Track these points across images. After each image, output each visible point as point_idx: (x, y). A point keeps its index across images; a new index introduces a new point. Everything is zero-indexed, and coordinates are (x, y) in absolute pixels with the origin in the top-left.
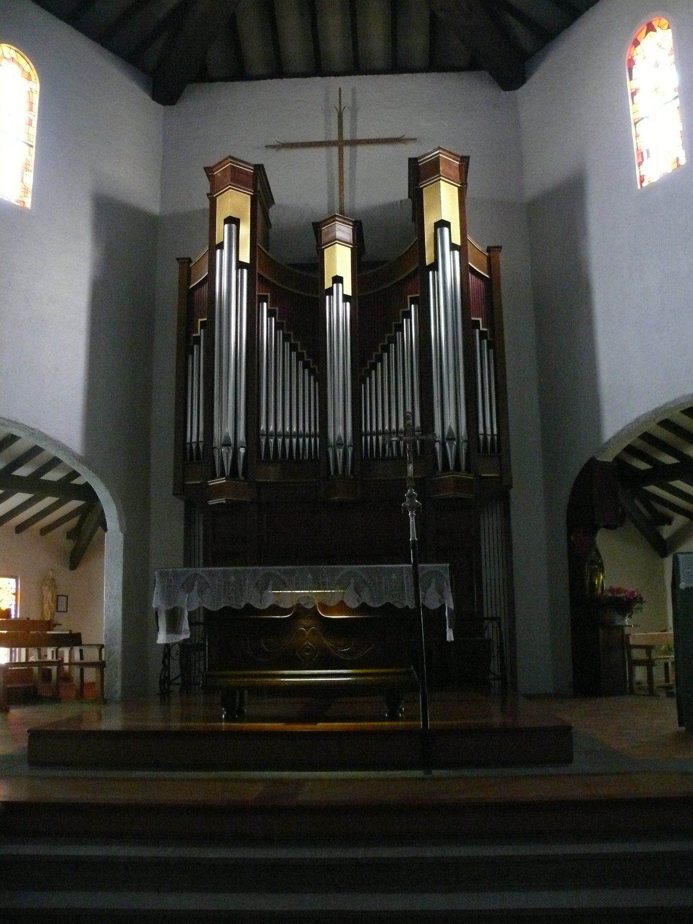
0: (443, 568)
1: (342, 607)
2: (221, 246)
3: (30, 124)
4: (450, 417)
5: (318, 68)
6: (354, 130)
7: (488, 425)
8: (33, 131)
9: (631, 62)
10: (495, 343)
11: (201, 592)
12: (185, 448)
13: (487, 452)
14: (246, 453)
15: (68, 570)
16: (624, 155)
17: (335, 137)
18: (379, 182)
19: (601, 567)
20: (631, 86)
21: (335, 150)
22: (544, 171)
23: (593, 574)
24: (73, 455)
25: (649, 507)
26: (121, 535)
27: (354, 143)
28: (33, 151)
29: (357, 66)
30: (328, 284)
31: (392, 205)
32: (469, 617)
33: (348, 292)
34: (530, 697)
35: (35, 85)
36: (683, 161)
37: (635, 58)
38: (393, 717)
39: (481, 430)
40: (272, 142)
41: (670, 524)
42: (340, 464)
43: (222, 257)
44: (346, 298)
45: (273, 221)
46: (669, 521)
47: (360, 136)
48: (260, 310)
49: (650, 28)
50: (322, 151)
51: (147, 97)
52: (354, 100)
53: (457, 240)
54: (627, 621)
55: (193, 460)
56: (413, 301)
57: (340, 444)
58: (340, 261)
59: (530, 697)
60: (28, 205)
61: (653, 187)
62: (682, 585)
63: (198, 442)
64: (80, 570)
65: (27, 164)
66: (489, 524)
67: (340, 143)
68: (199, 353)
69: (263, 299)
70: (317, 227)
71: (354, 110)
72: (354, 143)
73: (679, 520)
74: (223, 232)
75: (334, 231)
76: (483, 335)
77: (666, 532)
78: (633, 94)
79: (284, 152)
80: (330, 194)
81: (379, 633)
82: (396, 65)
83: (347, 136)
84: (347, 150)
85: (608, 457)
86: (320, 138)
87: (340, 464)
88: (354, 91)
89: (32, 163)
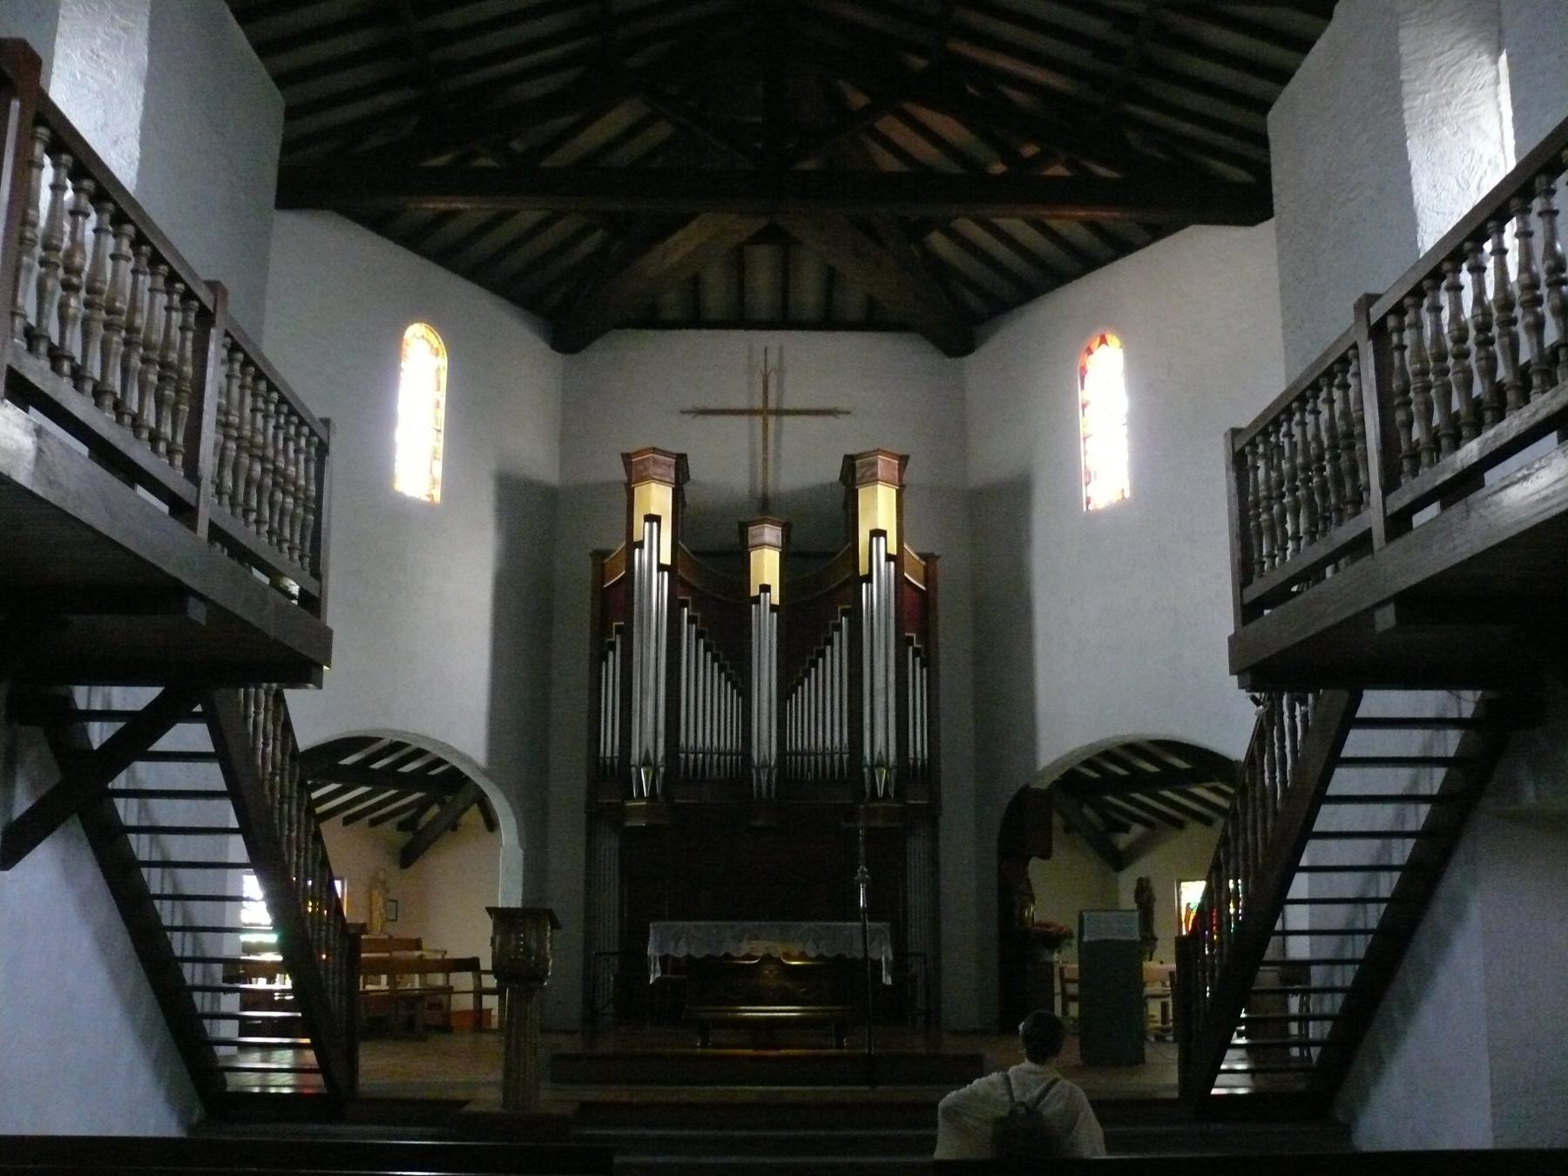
0: (884, 925)
1: (802, 956)
2: (640, 545)
3: (438, 406)
4: (880, 739)
5: (740, 320)
6: (780, 397)
7: (918, 744)
8: (441, 414)
9: (1083, 371)
10: (927, 630)
11: (688, 944)
12: (597, 764)
13: (919, 777)
14: (665, 774)
15: (396, 867)
16: (1070, 474)
17: (759, 404)
18: (805, 463)
19: (1032, 899)
20: (1083, 396)
21: (759, 420)
22: (991, 461)
23: (1024, 906)
24: (478, 768)
25: (1103, 816)
26: (520, 851)
27: (780, 412)
28: (441, 436)
29: (784, 320)
30: (754, 591)
31: (823, 487)
32: (900, 965)
33: (776, 600)
34: (955, 1033)
35: (443, 362)
36: (1127, 494)
37: (1088, 367)
38: (840, 1046)
39: (911, 755)
40: (688, 406)
41: (1127, 831)
42: (764, 786)
43: (641, 557)
44: (773, 608)
45: (688, 500)
46: (1126, 829)
47: (787, 405)
48: (681, 614)
49: (1103, 341)
50: (743, 421)
51: (543, 346)
52: (781, 359)
53: (893, 550)
54: (1056, 957)
55: (609, 777)
56: (844, 613)
57: (766, 765)
58: (767, 566)
59: (955, 1033)
60: (437, 498)
61: (1098, 514)
62: (1086, 939)
63: (612, 758)
64: (412, 870)
65: (435, 452)
66: (916, 846)
67: (765, 412)
68: (614, 660)
69: (684, 604)
70: (743, 529)
71: (781, 371)
72: (780, 412)
73: (1137, 830)
74: (641, 529)
75: (762, 534)
76: (916, 653)
77: (1123, 841)
78: (1084, 406)
79: (700, 421)
80: (753, 473)
81: (836, 979)
82: (828, 321)
83: (772, 405)
84: (772, 420)
85: (1043, 784)
86: (742, 405)
87: (764, 786)
88: (781, 348)
89: (441, 451)
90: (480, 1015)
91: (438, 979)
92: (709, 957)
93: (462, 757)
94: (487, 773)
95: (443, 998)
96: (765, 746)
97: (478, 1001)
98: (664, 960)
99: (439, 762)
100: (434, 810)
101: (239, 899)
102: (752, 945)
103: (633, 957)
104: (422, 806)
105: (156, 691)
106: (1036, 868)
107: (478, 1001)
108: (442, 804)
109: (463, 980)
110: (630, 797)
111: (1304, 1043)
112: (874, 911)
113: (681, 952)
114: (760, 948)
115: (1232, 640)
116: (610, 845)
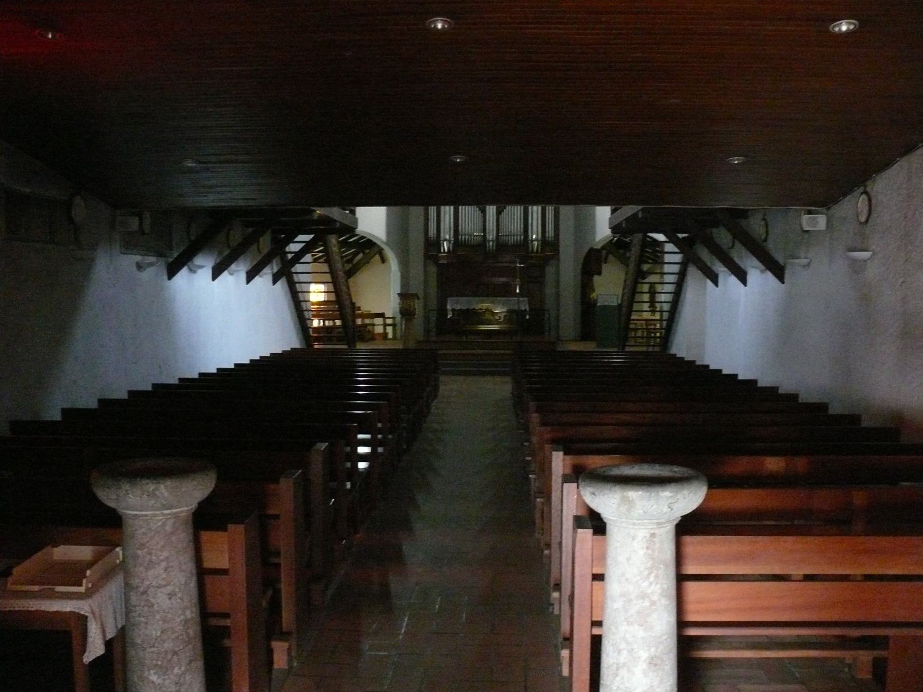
24: (382, 242)
66: (550, 270)
85: (599, 247)
90: (385, 335)
91: (367, 321)
92: (468, 310)
93: (377, 238)
94: (387, 244)
95: (362, 329)
96: (491, 236)
97: (385, 329)
98: (453, 310)
99: (363, 237)
100: (361, 256)
101: (309, 292)
102: (483, 305)
103: (442, 310)
104: (355, 255)
105: (312, 236)
106: (596, 278)
107: (385, 329)
108: (364, 253)
109: (379, 321)
110: (440, 252)
111: (655, 338)
112: (521, 294)
113: (459, 307)
114: (485, 305)
115: (610, 219)
116: (433, 269)
